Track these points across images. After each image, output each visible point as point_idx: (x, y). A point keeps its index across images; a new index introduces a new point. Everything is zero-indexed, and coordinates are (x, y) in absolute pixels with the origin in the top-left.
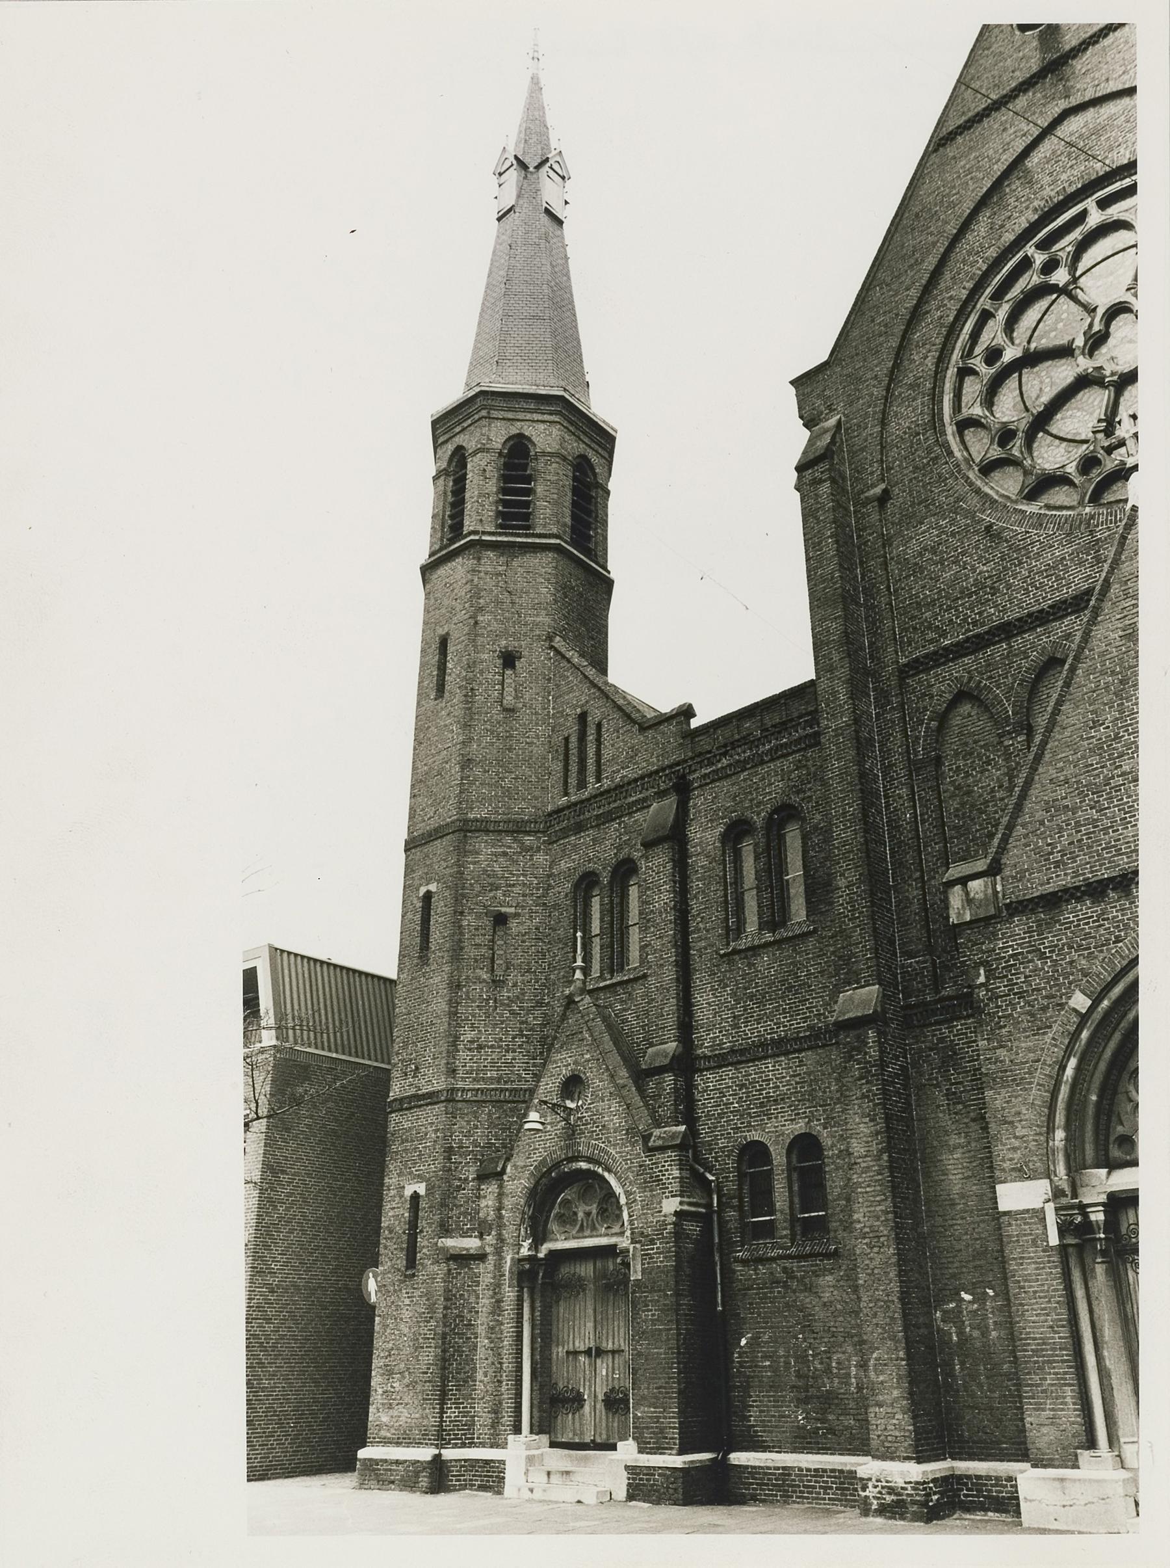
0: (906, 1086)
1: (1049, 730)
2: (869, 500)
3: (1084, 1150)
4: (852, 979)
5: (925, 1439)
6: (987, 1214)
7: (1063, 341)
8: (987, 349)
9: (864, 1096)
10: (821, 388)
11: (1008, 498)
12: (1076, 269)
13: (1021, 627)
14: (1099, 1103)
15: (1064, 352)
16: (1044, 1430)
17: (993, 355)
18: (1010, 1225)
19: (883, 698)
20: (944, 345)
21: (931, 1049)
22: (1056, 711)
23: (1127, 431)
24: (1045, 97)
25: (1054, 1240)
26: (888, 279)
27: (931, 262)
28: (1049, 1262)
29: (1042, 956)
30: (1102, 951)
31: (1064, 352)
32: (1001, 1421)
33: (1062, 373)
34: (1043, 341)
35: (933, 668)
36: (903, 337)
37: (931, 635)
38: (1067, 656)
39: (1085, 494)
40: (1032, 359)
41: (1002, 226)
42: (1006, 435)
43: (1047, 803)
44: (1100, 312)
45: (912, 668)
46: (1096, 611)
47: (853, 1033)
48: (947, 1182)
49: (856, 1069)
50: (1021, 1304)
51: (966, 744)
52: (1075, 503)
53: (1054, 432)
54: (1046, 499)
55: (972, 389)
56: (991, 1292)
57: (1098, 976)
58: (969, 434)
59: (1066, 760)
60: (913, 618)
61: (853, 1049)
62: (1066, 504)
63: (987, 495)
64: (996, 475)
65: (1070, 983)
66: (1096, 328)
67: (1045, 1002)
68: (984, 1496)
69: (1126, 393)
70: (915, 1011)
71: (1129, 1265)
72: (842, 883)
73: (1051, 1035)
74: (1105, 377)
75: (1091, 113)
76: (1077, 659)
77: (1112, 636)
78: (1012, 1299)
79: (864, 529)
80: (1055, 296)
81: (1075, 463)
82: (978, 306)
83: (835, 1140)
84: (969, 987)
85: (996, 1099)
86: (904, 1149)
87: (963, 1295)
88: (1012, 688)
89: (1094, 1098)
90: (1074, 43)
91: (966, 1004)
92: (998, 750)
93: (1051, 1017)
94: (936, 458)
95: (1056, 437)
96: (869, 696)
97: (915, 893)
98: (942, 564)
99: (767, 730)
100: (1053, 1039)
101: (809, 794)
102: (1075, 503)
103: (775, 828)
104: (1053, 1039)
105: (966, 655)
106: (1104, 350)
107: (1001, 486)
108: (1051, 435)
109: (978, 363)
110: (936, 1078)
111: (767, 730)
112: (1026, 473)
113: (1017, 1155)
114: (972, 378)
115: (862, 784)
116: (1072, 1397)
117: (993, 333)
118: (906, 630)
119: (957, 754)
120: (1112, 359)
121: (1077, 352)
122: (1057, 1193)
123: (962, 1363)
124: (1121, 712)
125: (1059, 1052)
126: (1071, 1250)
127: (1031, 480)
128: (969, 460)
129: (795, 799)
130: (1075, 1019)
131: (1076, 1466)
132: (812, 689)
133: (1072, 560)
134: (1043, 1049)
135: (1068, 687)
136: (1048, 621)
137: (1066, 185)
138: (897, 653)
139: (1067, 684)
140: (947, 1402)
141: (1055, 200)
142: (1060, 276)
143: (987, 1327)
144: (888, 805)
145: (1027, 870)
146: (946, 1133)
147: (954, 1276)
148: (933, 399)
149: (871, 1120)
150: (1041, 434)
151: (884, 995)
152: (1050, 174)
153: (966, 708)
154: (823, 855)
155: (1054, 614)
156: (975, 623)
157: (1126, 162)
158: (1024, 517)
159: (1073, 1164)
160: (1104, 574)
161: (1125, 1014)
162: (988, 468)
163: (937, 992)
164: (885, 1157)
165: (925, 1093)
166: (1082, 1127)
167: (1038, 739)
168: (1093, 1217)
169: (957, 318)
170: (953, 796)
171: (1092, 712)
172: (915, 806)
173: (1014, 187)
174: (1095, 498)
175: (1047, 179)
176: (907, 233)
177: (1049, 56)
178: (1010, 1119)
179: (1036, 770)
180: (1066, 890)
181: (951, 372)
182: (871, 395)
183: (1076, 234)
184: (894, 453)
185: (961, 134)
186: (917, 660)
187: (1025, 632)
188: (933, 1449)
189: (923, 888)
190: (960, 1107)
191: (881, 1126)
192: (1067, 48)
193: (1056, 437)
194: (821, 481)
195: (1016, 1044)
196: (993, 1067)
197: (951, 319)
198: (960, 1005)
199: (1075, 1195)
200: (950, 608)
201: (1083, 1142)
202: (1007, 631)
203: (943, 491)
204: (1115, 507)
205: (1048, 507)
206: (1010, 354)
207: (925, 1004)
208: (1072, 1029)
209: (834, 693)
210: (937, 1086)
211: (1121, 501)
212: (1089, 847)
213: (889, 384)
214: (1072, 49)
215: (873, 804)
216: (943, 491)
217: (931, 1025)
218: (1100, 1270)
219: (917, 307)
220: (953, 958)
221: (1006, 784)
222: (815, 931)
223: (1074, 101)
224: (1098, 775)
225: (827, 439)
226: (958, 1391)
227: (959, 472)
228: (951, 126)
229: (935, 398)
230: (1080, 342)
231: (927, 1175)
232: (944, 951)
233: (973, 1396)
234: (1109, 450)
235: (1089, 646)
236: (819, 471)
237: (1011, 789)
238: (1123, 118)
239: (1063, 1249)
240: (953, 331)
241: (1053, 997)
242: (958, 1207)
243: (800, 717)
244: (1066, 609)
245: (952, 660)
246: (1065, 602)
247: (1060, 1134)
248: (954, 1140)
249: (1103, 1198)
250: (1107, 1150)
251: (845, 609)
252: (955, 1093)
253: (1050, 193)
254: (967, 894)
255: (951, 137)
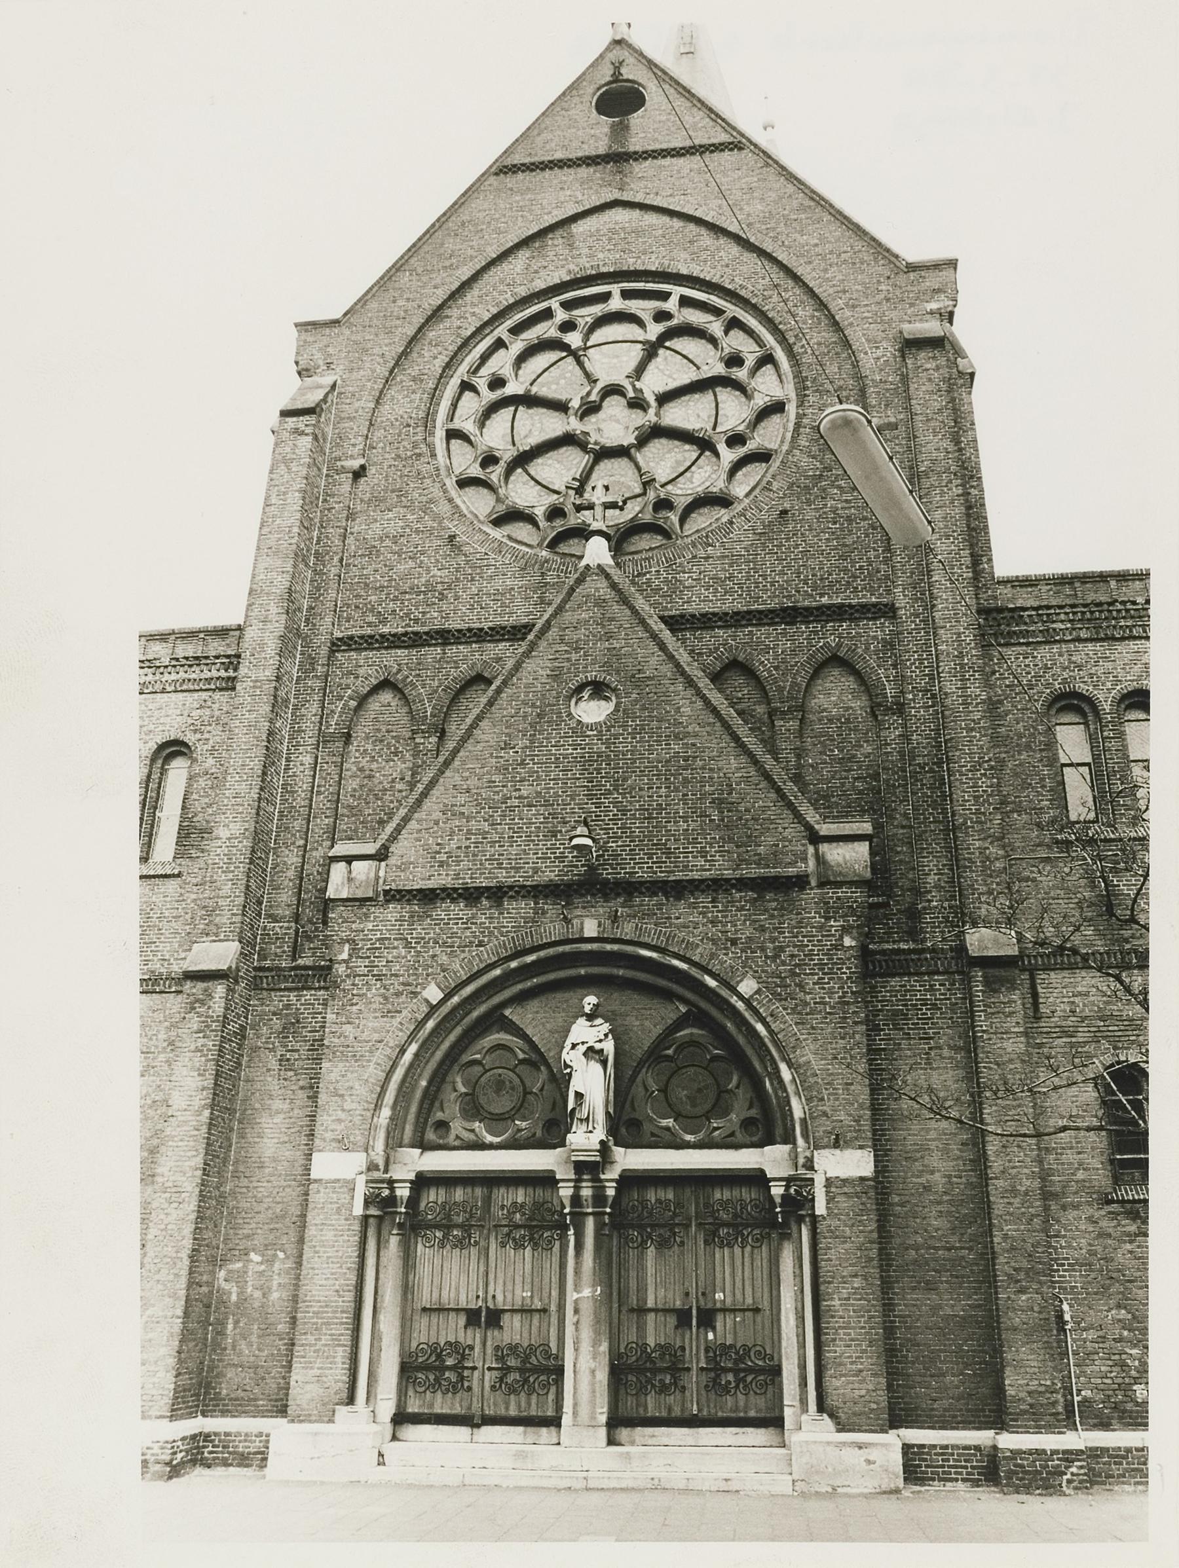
0: (240, 1047)
1: (464, 740)
2: (343, 470)
3: (404, 1129)
4: (211, 932)
5: (183, 1397)
6: (295, 1180)
7: (563, 397)
8: (493, 374)
9: (197, 1050)
10: (325, 343)
11: (476, 516)
12: (588, 340)
13: (458, 638)
14: (427, 1088)
15: (560, 407)
16: (308, 1387)
17: (497, 382)
18: (318, 1192)
19: (309, 664)
20: (456, 354)
21: (274, 1014)
22: (474, 726)
23: (598, 499)
24: (602, 179)
25: (358, 1209)
26: (420, 270)
27: (465, 273)
28: (349, 1230)
29: (408, 946)
30: (463, 951)
31: (560, 407)
32: (263, 1378)
33: (551, 425)
34: (544, 389)
35: (365, 649)
36: (420, 330)
37: (371, 618)
38: (496, 677)
39: (545, 539)
40: (529, 400)
41: (536, 272)
42: (489, 460)
43: (446, 805)
44: (600, 385)
45: (345, 644)
46: (533, 646)
47: (201, 985)
48: (261, 1145)
49: (194, 1022)
50: (313, 1268)
51: (379, 730)
52: (535, 543)
53: (533, 473)
54: (508, 529)
55: (470, 405)
56: (281, 1255)
57: (455, 973)
58: (455, 444)
59: (472, 771)
60: (358, 596)
61: (197, 1001)
62: (525, 540)
63: (457, 506)
64: (471, 491)
65: (428, 975)
66: (593, 397)
67: (401, 988)
68: (229, 1453)
69: (602, 464)
70: (266, 974)
71: (420, 1239)
72: (223, 833)
73: (399, 1020)
74: (588, 443)
75: (637, 213)
76: (505, 683)
77: (541, 672)
78: (305, 1263)
79: (333, 496)
80: (564, 354)
81: (544, 508)
82: (496, 332)
83: (150, 1090)
84: (331, 960)
85: (332, 1071)
86: (226, 1108)
87: (253, 1256)
88: (436, 691)
89: (424, 1083)
90: (638, 148)
91: (322, 975)
92: (407, 745)
93: (403, 1003)
94: (420, 455)
95: (532, 478)
96: (295, 657)
97: (295, 859)
98: (400, 556)
99: (177, 660)
100: (401, 1023)
101: (206, 736)
102: (535, 543)
103: (160, 761)
104: (401, 1023)
105: (399, 647)
106: (593, 419)
107: (472, 504)
108: (529, 475)
109: (481, 383)
110: (273, 1043)
111: (177, 660)
112: (498, 500)
113: (340, 1127)
114: (472, 394)
115: (269, 742)
116: (343, 1357)
117: (501, 363)
118: (349, 606)
119: (367, 738)
120: (599, 430)
121: (571, 412)
122: (372, 1167)
123: (236, 1322)
124: (532, 742)
125: (403, 1037)
126: (371, 1220)
127: (501, 508)
128: (449, 469)
129: (190, 738)
130: (425, 1009)
131: (331, 1421)
132: (237, 633)
133: (519, 593)
134: (388, 1032)
135: (491, 706)
136: (484, 641)
137: (601, 263)
138: (333, 624)
139: (491, 703)
140: (212, 1361)
141: (588, 272)
142: (574, 339)
143: (270, 1289)
144: (287, 769)
145: (411, 863)
146: (271, 1097)
147: (248, 1237)
148: (432, 399)
149: (199, 1075)
150: (519, 470)
151: (241, 953)
152: (590, 248)
153: (386, 696)
154: (207, 800)
155: (491, 636)
156: (416, 621)
157: (654, 269)
158: (487, 540)
159: (390, 1141)
160: (546, 616)
161: (470, 1012)
162: (465, 483)
163: (294, 959)
164: (207, 1113)
165: (259, 1056)
166: (407, 1110)
167: (451, 745)
168: (398, 1192)
169: (473, 335)
170: (354, 776)
171: (508, 735)
172: (314, 776)
173: (556, 242)
174: (553, 545)
175: (585, 251)
176: (449, 235)
177: (614, 147)
178: (341, 1092)
179: (443, 773)
180: (444, 890)
181: (455, 382)
182: (373, 371)
183: (597, 310)
184: (380, 433)
185: (523, 171)
186: (351, 638)
187: (461, 643)
188: (187, 1407)
189: (304, 856)
190: (292, 1073)
191: (210, 1083)
192: (632, 149)
193: (532, 478)
194: (302, 433)
195: (363, 1022)
196: (336, 1040)
197: (469, 333)
198: (314, 976)
199: (386, 1171)
200: (396, 599)
201: (405, 1123)
202: (445, 637)
203: (418, 488)
204: (568, 560)
205: (510, 538)
206: (513, 388)
207: (279, 969)
208: (420, 1017)
209: (262, 645)
210: (273, 1050)
211: (573, 556)
212: (474, 855)
213: (394, 368)
214: (636, 153)
215: (273, 763)
216: (418, 488)
217: (280, 990)
218: (394, 1241)
219: (441, 307)
220: (317, 929)
221: (408, 778)
222: (179, 875)
223: (626, 197)
224: (498, 793)
225: (319, 395)
226: (225, 1349)
227: (438, 476)
228: (518, 159)
229: (434, 397)
230: (575, 404)
231: (242, 1136)
232: (310, 921)
233: (240, 1354)
234: (579, 508)
235: (519, 675)
236: (301, 422)
237: (412, 785)
238: (660, 232)
239: (366, 1218)
240: (466, 344)
241: (409, 985)
242: (267, 1171)
243: (217, 657)
244: (503, 635)
245: (386, 648)
246: (504, 628)
247: (386, 1112)
248: (277, 1104)
249: (412, 1176)
250: (423, 1133)
251: (295, 566)
252: (288, 1060)
253: (585, 264)
254: (350, 872)
255: (514, 169)
